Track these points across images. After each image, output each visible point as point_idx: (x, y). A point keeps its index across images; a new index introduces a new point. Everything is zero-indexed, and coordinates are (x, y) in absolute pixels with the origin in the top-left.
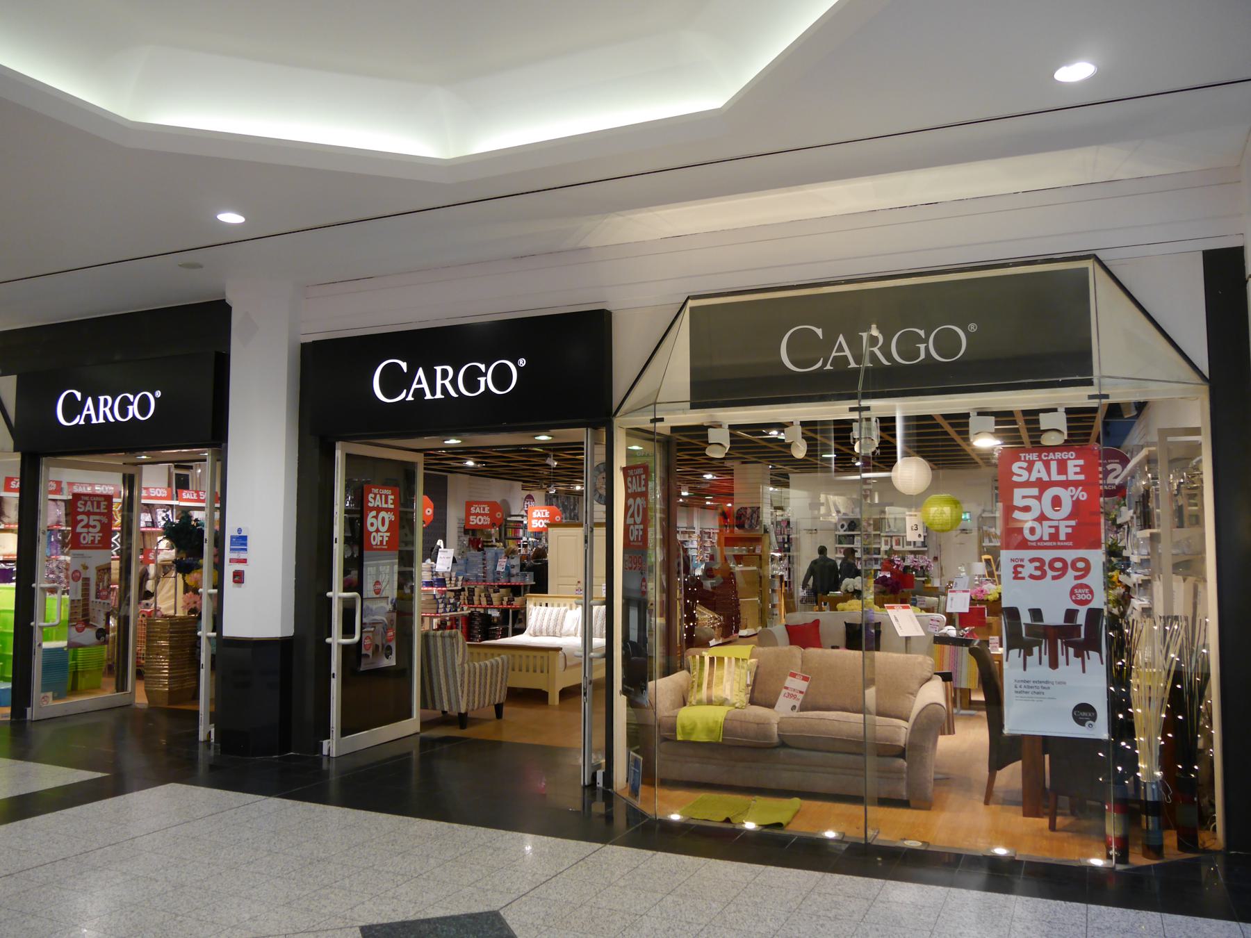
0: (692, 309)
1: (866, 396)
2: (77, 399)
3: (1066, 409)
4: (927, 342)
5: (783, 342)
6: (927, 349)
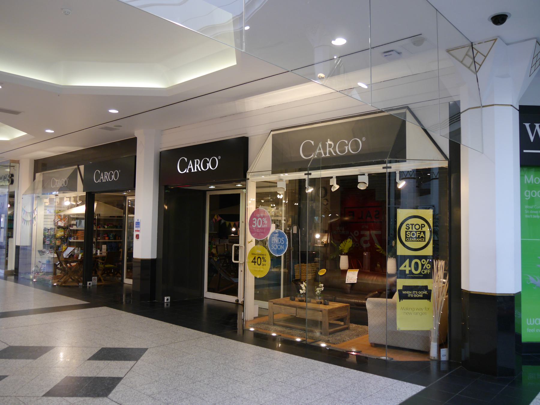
0: (273, 135)
1: (390, 162)
3: (368, 174)
4: (348, 146)
6: (349, 149)
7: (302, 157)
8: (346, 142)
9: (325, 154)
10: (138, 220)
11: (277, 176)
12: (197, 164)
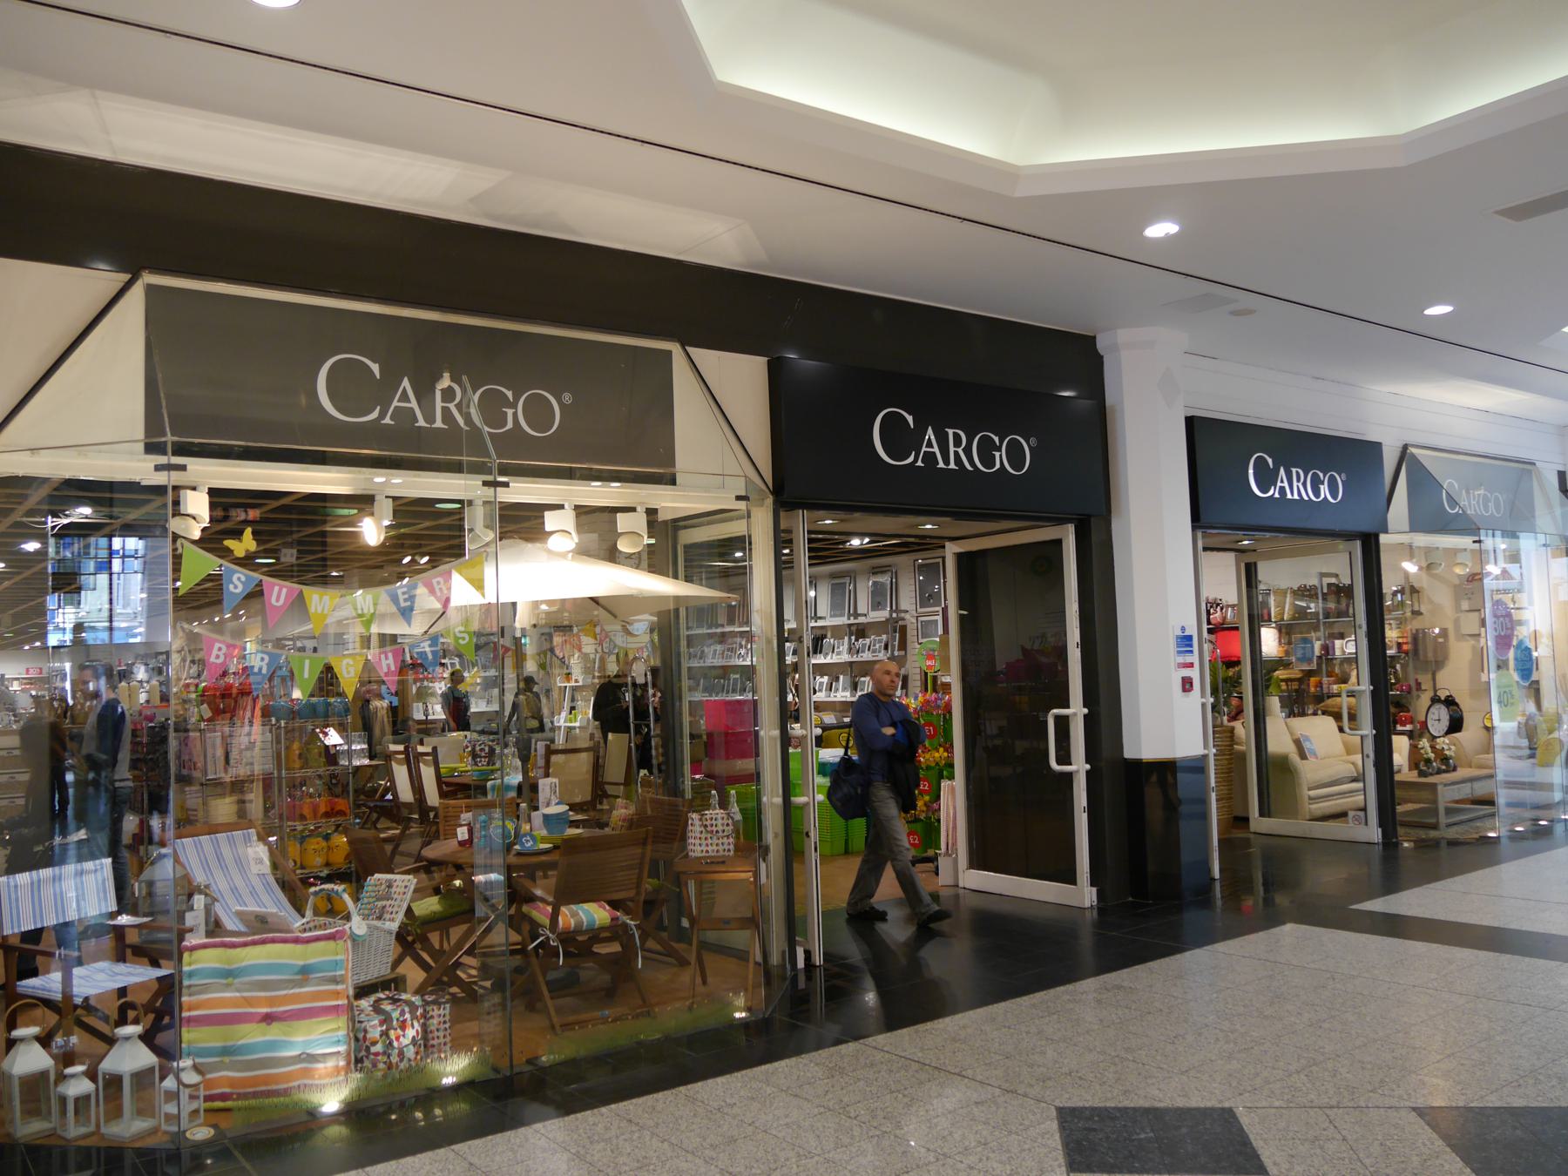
2: (375, 376)
3: (209, 489)
5: (321, 372)
7: (325, 411)
8: (996, 439)
9: (430, 418)
10: (1183, 629)
11: (362, 476)
12: (1298, 480)
